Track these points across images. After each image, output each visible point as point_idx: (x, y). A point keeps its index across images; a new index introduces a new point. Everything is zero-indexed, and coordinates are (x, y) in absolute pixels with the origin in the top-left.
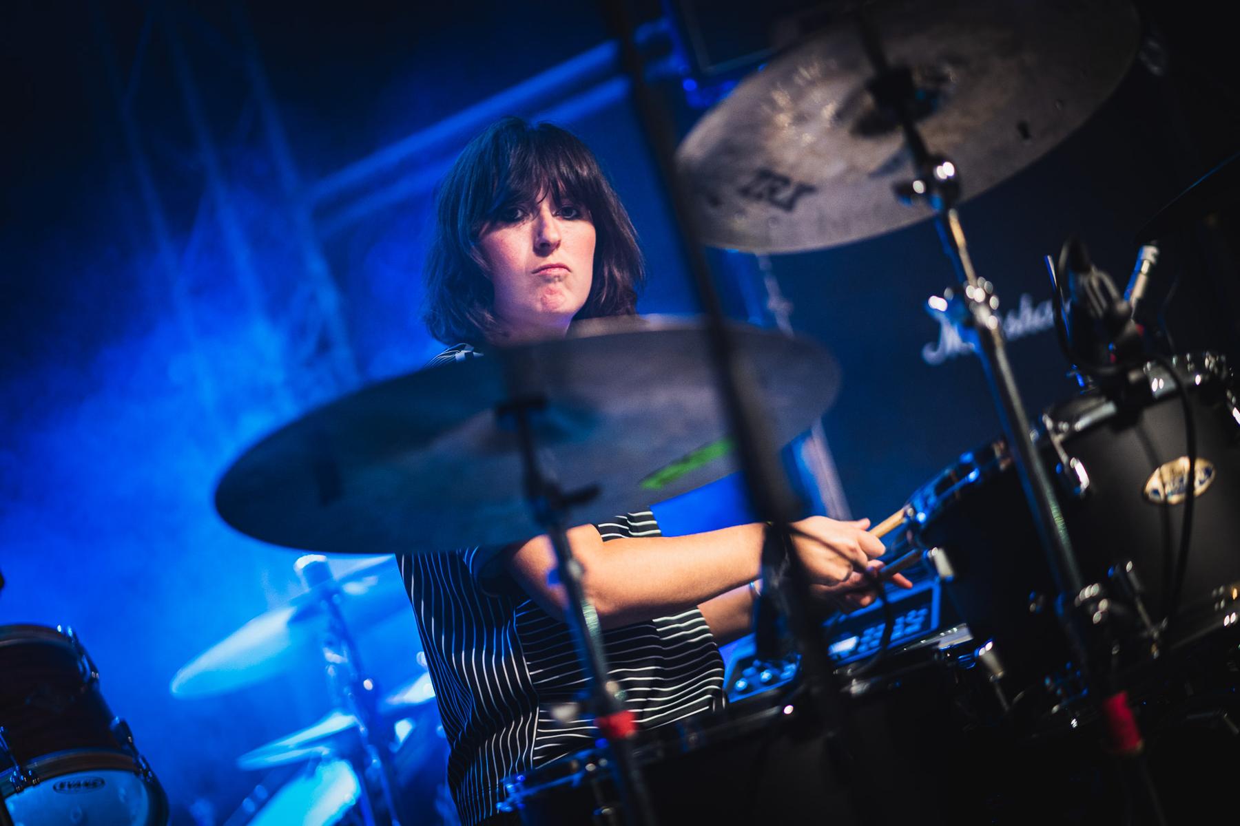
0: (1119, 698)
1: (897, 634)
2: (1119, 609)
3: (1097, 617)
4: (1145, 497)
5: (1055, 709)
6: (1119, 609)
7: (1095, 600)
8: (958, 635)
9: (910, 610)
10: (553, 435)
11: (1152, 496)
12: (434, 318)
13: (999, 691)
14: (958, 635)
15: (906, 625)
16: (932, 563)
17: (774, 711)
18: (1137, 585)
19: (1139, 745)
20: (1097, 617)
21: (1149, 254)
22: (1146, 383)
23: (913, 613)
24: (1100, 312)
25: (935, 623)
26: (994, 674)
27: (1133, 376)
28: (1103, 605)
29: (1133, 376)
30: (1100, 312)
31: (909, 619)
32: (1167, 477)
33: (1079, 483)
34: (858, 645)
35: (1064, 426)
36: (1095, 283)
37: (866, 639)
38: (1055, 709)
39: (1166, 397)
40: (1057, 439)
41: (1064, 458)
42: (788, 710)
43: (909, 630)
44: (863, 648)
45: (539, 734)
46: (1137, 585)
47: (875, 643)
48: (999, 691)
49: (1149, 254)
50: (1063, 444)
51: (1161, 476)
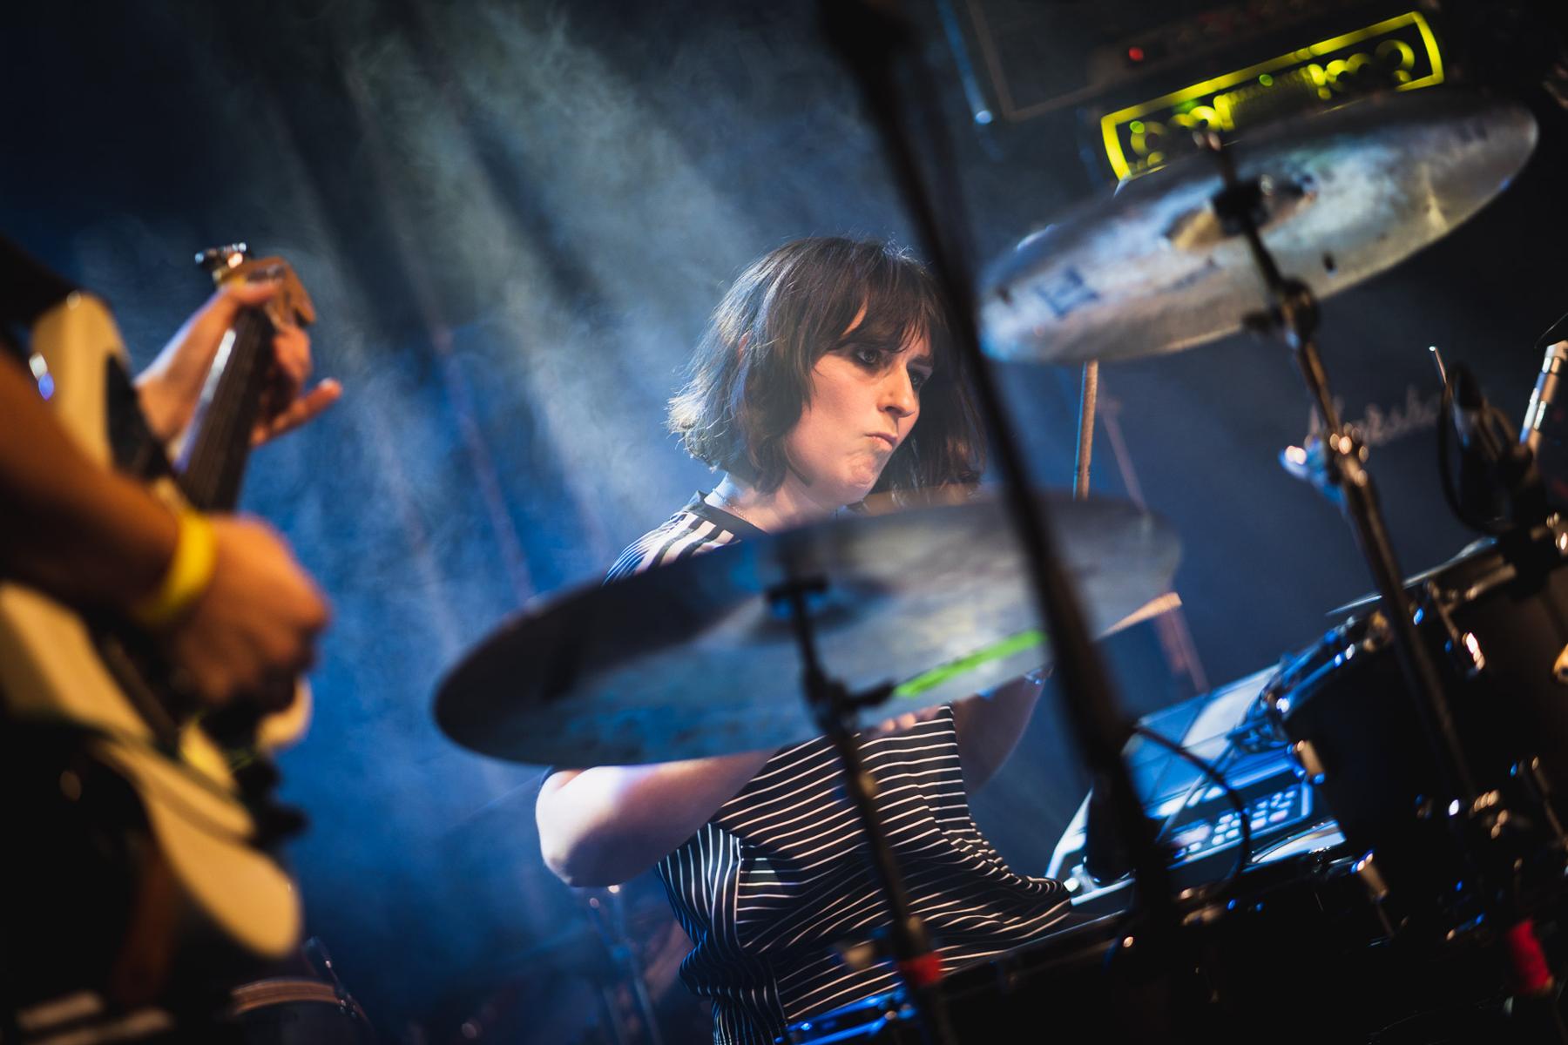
0: (1524, 928)
1: (1255, 825)
2: (1521, 822)
3: (1495, 831)
5: (1451, 934)
6: (1521, 822)
7: (1493, 811)
9: (1276, 792)
10: (840, 616)
13: (1381, 913)
15: (1271, 811)
16: (1399, 54)
17: (1111, 944)
18: (1545, 786)
20: (1495, 831)
23: (1278, 796)
24: (1494, 457)
25: (1305, 811)
26: (1376, 893)
27: (1536, 534)
28: (1503, 817)
29: (1536, 534)
30: (1494, 457)
31: (1274, 804)
33: (1474, 664)
35: (1453, 595)
37: (1219, 829)
38: (1451, 934)
40: (1445, 610)
41: (1454, 633)
42: (1128, 941)
43: (1275, 817)
44: (1217, 840)
45: (744, 879)
46: (1545, 786)
47: (1234, 833)
48: (1381, 913)
50: (1453, 615)
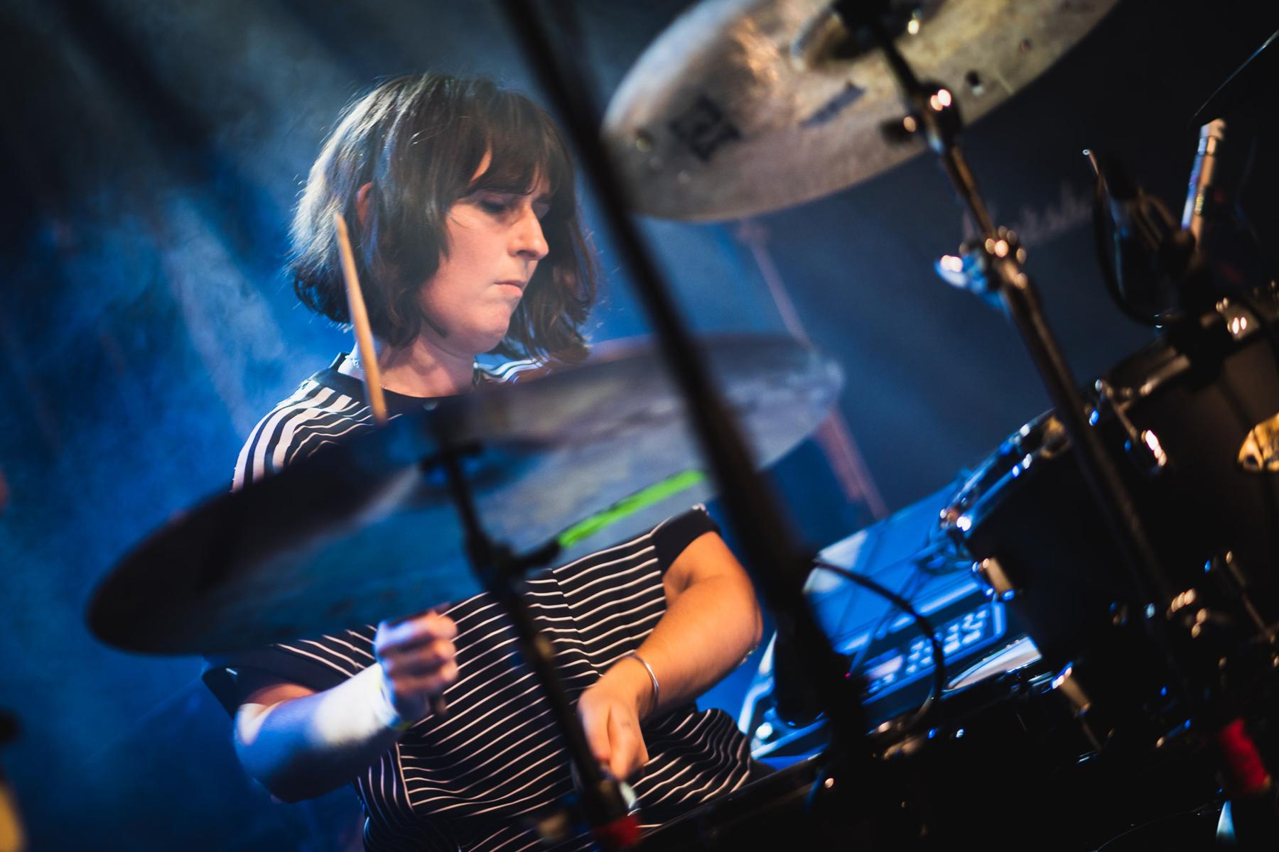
0: (1235, 730)
1: (948, 649)
2: (1221, 619)
4: (1239, 466)
5: (1160, 742)
6: (1221, 619)
7: (1190, 609)
8: (1023, 652)
10: (497, 477)
11: (1246, 465)
12: (367, 174)
13: (1086, 728)
14: (1023, 652)
15: (964, 633)
18: (1242, 581)
19: (1267, 781)
21: (1211, 132)
22: (1222, 323)
23: (969, 618)
25: (999, 629)
27: (1206, 321)
28: (1202, 616)
29: (1206, 321)
31: (966, 626)
32: (1263, 441)
33: (1156, 460)
34: (906, 664)
36: (1144, 209)
37: (914, 657)
38: (1160, 742)
39: (1249, 338)
40: (1121, 409)
41: (1132, 432)
43: (968, 640)
44: (912, 669)
47: (927, 660)
48: (1086, 728)
49: (1211, 132)
50: (1128, 413)
51: (1256, 438)
